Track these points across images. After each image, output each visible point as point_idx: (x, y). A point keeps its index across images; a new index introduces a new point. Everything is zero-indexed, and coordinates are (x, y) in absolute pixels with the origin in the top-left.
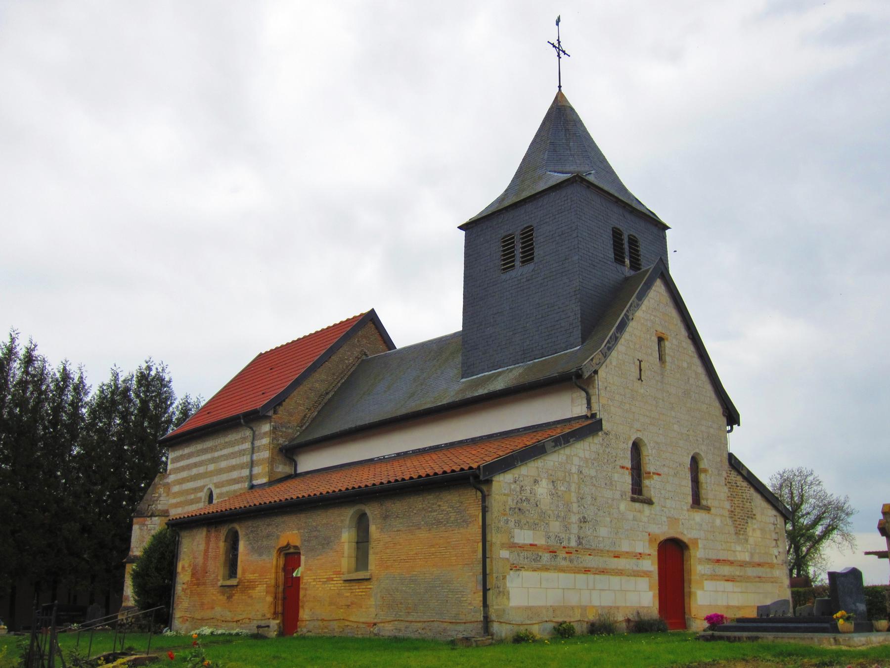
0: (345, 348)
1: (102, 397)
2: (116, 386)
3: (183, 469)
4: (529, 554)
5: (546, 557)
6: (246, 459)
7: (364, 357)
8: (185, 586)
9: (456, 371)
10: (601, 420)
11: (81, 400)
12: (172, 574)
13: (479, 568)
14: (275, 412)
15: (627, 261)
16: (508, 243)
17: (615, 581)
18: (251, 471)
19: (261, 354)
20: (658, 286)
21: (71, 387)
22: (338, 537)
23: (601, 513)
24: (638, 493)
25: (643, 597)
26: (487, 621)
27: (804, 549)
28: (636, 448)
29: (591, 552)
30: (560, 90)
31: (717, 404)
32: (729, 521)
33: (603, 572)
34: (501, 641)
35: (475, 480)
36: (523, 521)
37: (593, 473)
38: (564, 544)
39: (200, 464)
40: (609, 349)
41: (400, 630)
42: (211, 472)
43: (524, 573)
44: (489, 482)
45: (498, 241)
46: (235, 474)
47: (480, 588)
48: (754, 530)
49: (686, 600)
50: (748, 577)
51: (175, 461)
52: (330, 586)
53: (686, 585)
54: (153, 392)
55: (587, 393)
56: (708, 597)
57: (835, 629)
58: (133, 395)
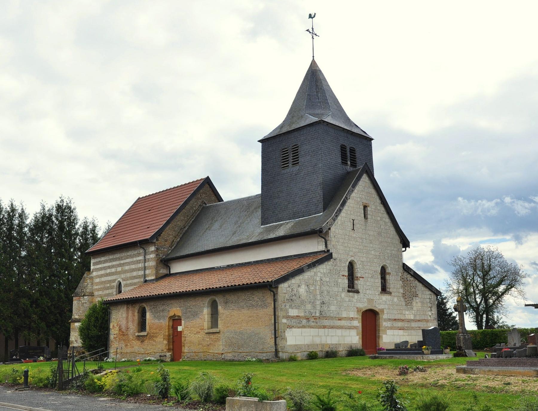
0: (193, 200)
1: (36, 220)
2: (45, 214)
3: (101, 269)
4: (296, 320)
5: (304, 322)
6: (141, 265)
7: (204, 205)
8: (115, 336)
9: (258, 221)
10: (332, 253)
11: (24, 223)
12: (108, 329)
13: (273, 327)
14: (157, 240)
15: (349, 163)
16: (285, 152)
17: (339, 332)
18: (145, 272)
19: (140, 201)
20: (365, 178)
21: (17, 215)
22: (202, 312)
23: (332, 299)
24: (352, 287)
25: (354, 339)
26: (277, 352)
27: (491, 301)
28: (351, 266)
29: (326, 318)
30: (313, 59)
31: (397, 237)
32: (402, 299)
33: (332, 327)
34: (283, 361)
35: (270, 287)
36: (293, 305)
37: (328, 280)
38: (313, 315)
39: (113, 267)
40: (337, 216)
41: (235, 356)
42: (119, 272)
43: (294, 329)
44: (277, 288)
45: (279, 149)
46: (135, 274)
47: (273, 336)
48: (417, 302)
49: (377, 340)
50: (412, 328)
51: (96, 266)
52: (199, 335)
53: (377, 332)
54: (66, 216)
55: (325, 239)
56: (389, 338)
57: (423, 353)
58: (54, 219)
